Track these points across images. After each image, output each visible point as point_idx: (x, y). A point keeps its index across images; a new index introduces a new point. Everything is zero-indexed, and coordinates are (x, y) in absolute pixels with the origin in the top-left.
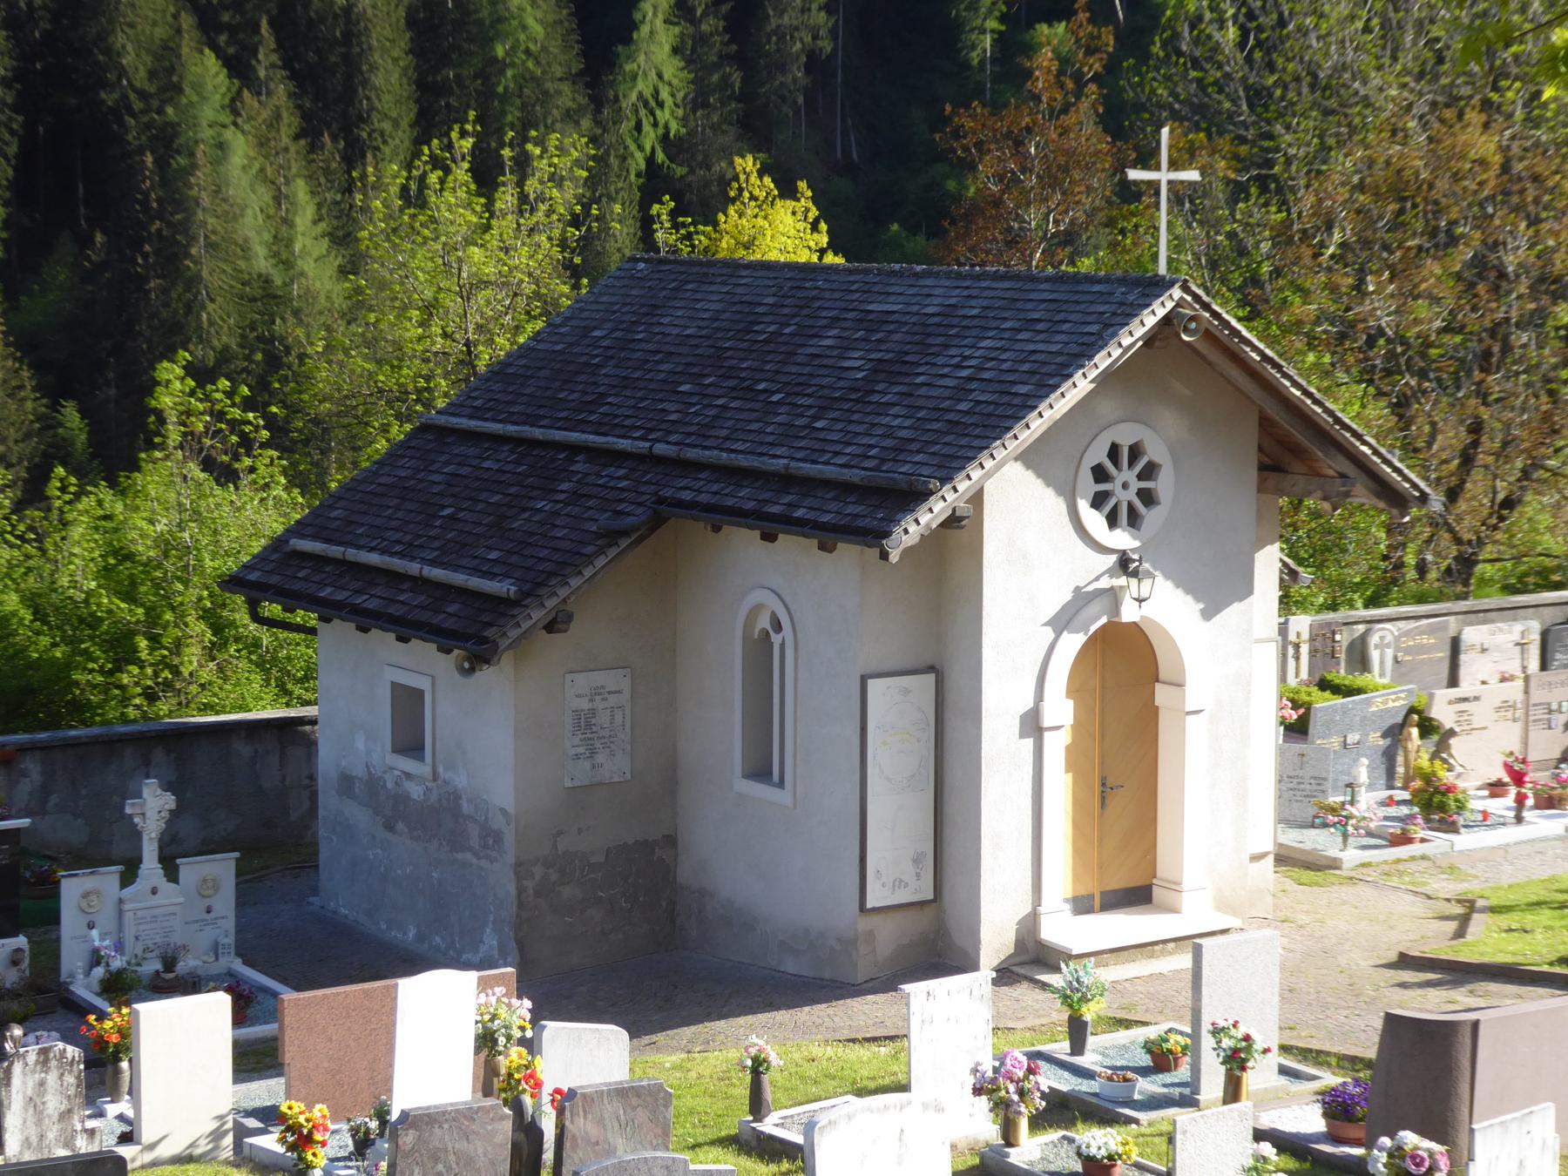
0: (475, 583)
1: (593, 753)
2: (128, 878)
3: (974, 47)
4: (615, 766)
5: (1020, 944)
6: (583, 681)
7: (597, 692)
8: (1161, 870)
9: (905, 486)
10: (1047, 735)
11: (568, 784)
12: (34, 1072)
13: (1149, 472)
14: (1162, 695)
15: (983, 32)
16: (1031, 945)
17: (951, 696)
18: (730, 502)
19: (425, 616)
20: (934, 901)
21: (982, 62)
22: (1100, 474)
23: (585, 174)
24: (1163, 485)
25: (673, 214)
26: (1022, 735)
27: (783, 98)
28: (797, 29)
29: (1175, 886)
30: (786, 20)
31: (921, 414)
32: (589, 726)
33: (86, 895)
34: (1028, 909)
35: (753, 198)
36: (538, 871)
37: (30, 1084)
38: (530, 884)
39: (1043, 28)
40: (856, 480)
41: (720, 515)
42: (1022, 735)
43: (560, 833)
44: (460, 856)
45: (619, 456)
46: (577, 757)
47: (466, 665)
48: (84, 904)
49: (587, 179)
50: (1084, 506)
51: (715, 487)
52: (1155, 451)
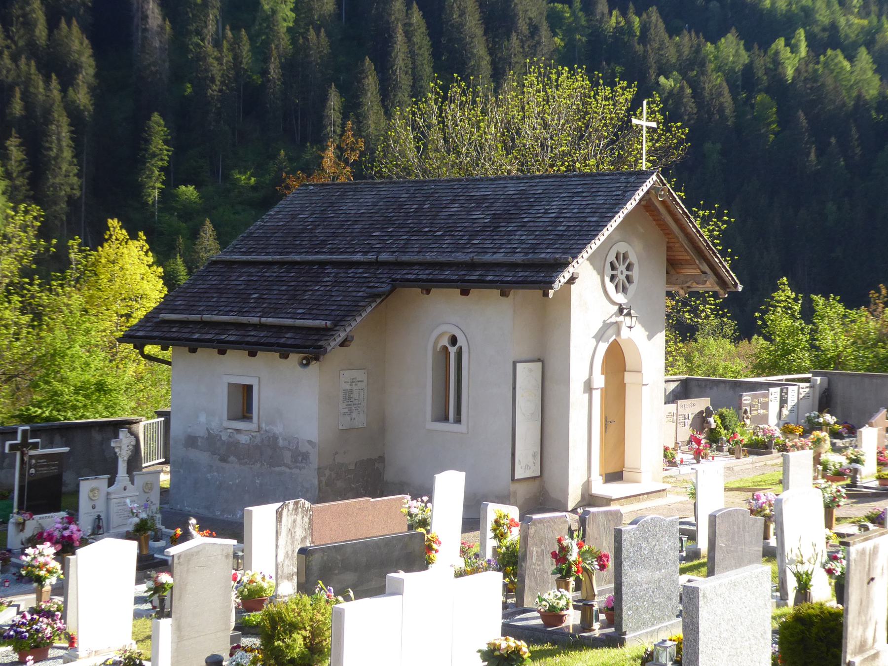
0: (299, 322)
1: (351, 412)
2: (111, 483)
3: (150, 196)
4: (360, 420)
5: (583, 496)
6: (348, 375)
7: (353, 381)
8: (628, 462)
9: (552, 261)
10: (594, 392)
11: (341, 428)
12: (291, 514)
13: (629, 267)
14: (628, 377)
15: (154, 188)
16: (586, 496)
17: (548, 374)
18: (442, 277)
19: (273, 340)
20: (541, 476)
21: (154, 203)
22: (613, 267)
23: (39, 224)
24: (635, 273)
25: (80, 245)
26: (584, 392)
27: (55, 217)
28: (62, 185)
29: (637, 470)
30: (57, 180)
31: (537, 233)
32: (350, 398)
33: (92, 490)
34: (586, 479)
35: (117, 239)
36: (327, 472)
37: (290, 521)
38: (323, 479)
39: (183, 188)
40: (519, 261)
41: (427, 285)
42: (584, 392)
43: (336, 453)
44: (277, 469)
45: (358, 264)
46: (344, 414)
47: (304, 362)
48: (91, 495)
49: (39, 227)
50: (607, 279)
51: (427, 272)
52: (633, 258)
